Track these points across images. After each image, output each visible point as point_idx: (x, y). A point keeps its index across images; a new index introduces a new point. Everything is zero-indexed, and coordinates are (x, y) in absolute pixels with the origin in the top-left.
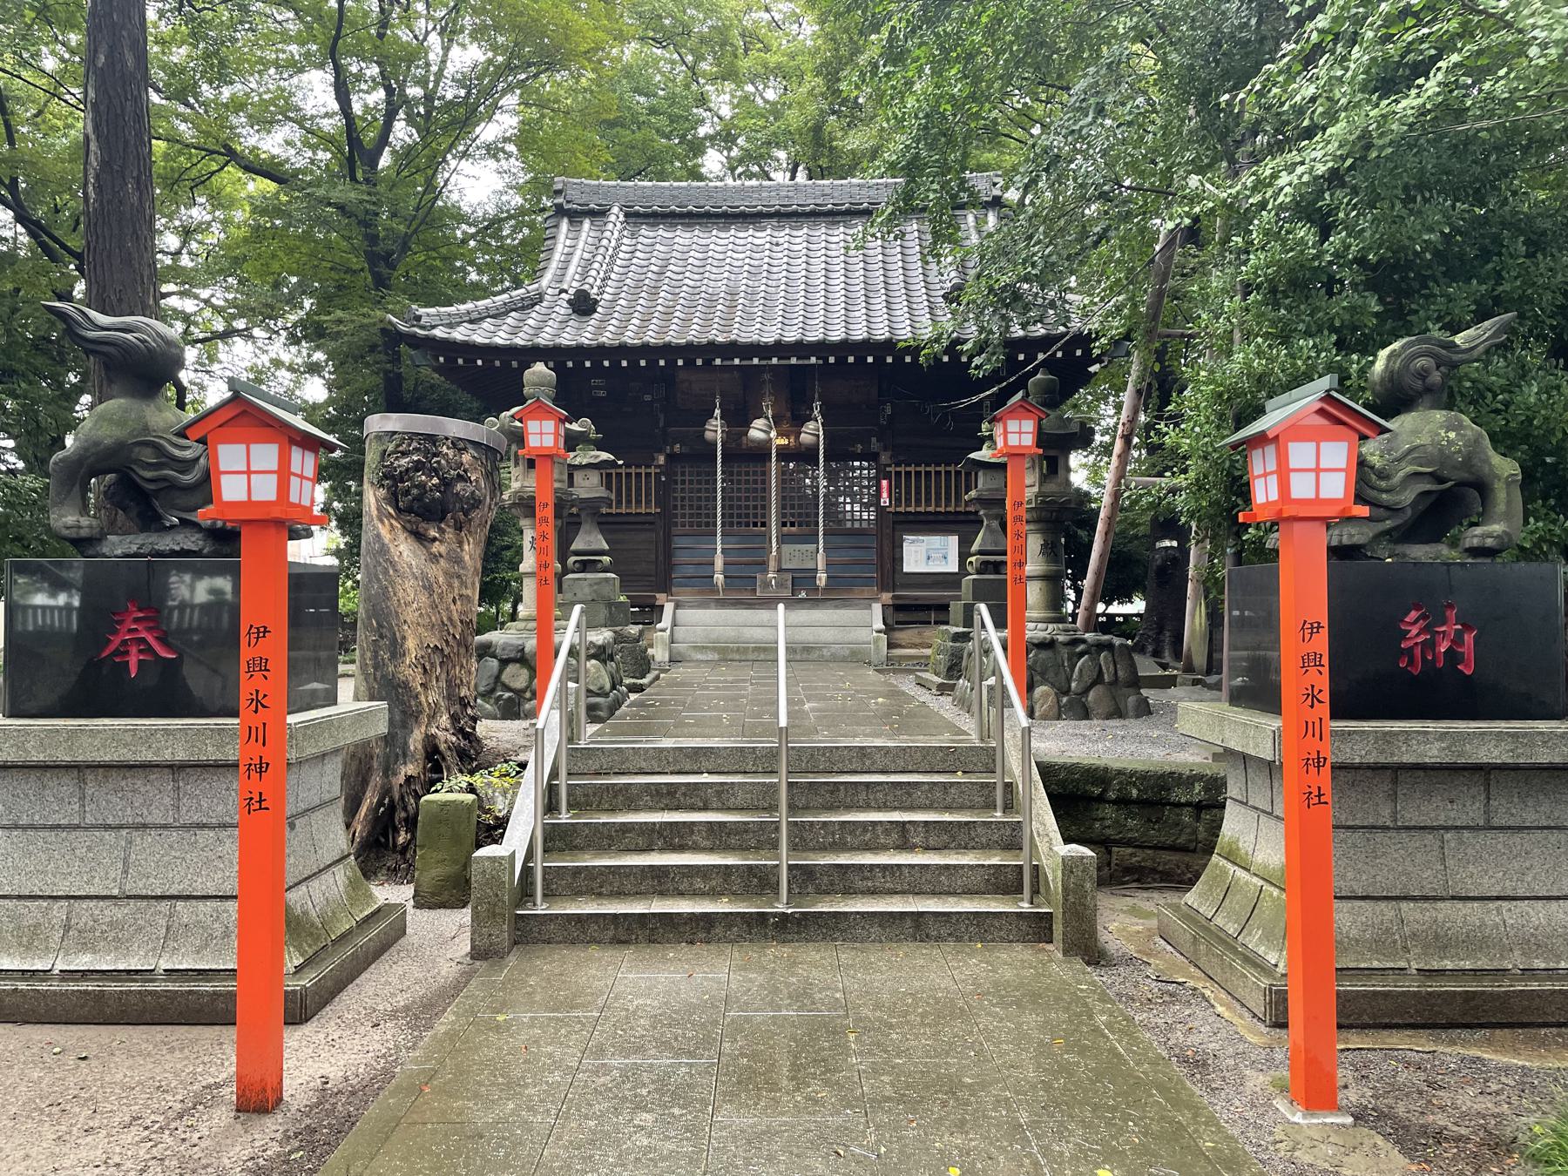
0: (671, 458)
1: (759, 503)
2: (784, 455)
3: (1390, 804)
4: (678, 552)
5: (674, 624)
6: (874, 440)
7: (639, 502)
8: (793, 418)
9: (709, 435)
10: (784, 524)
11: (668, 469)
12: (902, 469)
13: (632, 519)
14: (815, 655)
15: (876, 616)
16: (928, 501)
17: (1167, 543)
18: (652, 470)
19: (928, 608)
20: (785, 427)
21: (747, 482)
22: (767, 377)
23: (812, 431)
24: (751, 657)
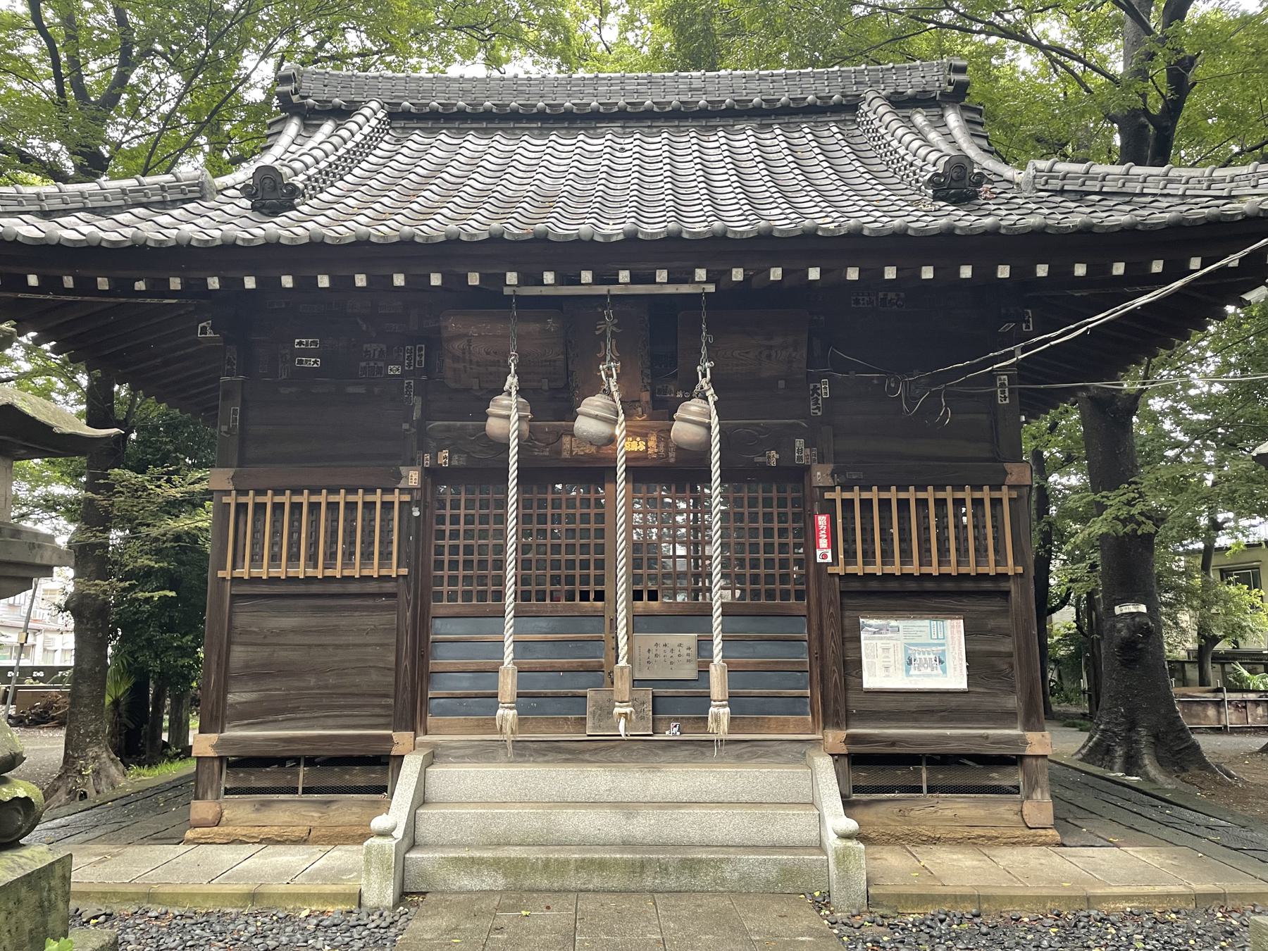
0: (433, 475)
1: (592, 557)
2: (641, 472)
3: (1028, 760)
4: (441, 650)
5: (422, 799)
6: (799, 443)
7: (367, 556)
8: (657, 398)
9: (494, 426)
10: (637, 596)
11: (426, 496)
12: (856, 495)
13: (353, 588)
14: (705, 879)
15: (826, 777)
16: (906, 555)
17: (1130, 608)
18: (395, 498)
19: (912, 760)
20: (639, 420)
21: (571, 518)
22: (609, 321)
23: (697, 419)
24: (574, 882)
